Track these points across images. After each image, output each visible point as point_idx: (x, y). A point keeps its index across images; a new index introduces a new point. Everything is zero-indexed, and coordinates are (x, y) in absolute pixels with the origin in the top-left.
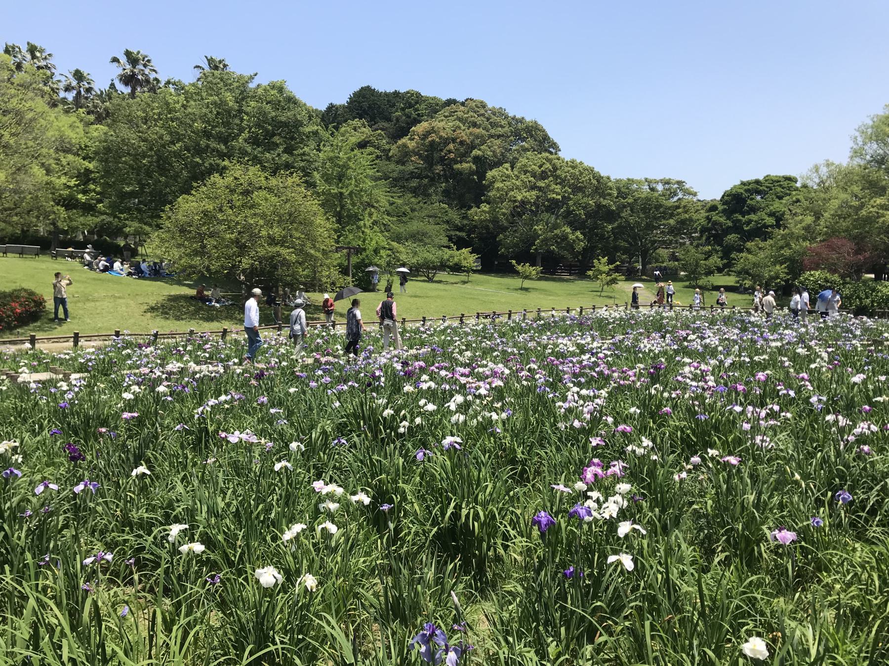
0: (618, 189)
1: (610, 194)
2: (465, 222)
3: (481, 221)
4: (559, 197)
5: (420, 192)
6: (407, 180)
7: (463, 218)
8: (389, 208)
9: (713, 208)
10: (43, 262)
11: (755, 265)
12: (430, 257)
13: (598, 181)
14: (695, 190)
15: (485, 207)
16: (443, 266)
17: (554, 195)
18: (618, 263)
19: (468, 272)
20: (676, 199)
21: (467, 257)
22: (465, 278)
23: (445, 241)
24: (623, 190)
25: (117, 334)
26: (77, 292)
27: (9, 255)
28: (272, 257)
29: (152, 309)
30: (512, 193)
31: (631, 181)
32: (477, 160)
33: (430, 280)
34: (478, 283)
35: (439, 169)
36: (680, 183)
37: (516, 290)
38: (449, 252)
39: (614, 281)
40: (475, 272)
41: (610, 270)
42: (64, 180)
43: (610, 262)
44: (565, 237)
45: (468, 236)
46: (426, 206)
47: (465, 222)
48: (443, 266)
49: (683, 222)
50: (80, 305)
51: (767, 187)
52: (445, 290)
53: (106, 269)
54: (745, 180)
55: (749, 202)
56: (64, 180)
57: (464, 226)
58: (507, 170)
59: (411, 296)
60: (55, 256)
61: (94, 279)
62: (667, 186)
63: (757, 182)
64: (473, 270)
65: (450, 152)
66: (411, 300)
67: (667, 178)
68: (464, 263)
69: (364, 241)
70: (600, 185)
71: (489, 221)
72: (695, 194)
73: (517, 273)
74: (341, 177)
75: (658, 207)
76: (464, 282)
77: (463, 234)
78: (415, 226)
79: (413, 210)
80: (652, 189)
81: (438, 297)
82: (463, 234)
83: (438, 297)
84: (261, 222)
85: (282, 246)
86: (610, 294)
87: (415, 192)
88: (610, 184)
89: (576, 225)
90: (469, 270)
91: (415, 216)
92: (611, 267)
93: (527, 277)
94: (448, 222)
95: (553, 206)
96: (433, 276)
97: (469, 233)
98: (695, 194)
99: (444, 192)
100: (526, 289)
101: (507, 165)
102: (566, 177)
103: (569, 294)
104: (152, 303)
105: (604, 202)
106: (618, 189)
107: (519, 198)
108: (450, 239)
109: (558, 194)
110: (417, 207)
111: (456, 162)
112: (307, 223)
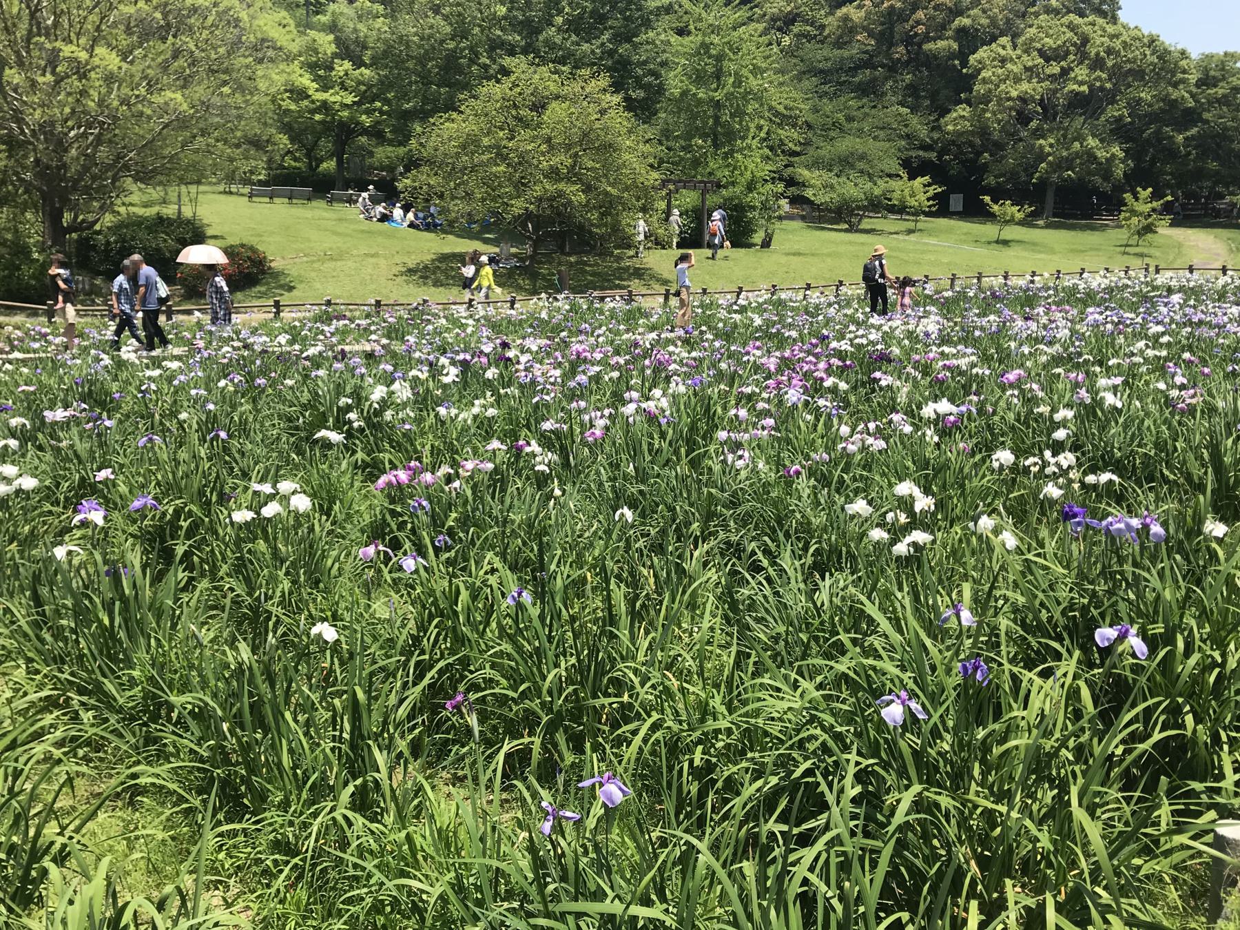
0: (1206, 71)
1: (1183, 81)
2: (936, 135)
3: (960, 134)
4: (1085, 88)
5: (867, 90)
7: (933, 129)
8: (811, 118)
15: (963, 110)
16: (878, 206)
17: (1075, 87)
18: (1169, 198)
19: (916, 214)
21: (919, 191)
22: (911, 225)
23: (893, 165)
25: (329, 303)
27: (276, 200)
28: (552, 199)
29: (411, 271)
32: (962, 33)
33: (852, 229)
35: (900, 51)
39: (1149, 229)
41: (1154, 210)
43: (1155, 196)
44: (1090, 156)
45: (939, 157)
47: (936, 135)
52: (850, 243)
53: (384, 218)
57: (936, 142)
58: (1004, 47)
60: (330, 202)
65: (918, 23)
66: (784, 259)
70: (1166, 65)
71: (972, 133)
74: (718, 75)
76: (910, 232)
77: (933, 155)
78: (845, 145)
79: (850, 119)
81: (829, 255)
83: (829, 255)
86: (1145, 251)
87: (864, 90)
88: (1184, 63)
90: (917, 213)
92: (1155, 204)
93: (1011, 221)
99: (908, 87)
100: (1006, 243)
101: (1004, 40)
103: (1072, 251)
105: (1175, 94)
107: (1014, 94)
108: (906, 164)
109: (1081, 83)
110: (858, 114)
111: (927, 38)
112: (608, 148)
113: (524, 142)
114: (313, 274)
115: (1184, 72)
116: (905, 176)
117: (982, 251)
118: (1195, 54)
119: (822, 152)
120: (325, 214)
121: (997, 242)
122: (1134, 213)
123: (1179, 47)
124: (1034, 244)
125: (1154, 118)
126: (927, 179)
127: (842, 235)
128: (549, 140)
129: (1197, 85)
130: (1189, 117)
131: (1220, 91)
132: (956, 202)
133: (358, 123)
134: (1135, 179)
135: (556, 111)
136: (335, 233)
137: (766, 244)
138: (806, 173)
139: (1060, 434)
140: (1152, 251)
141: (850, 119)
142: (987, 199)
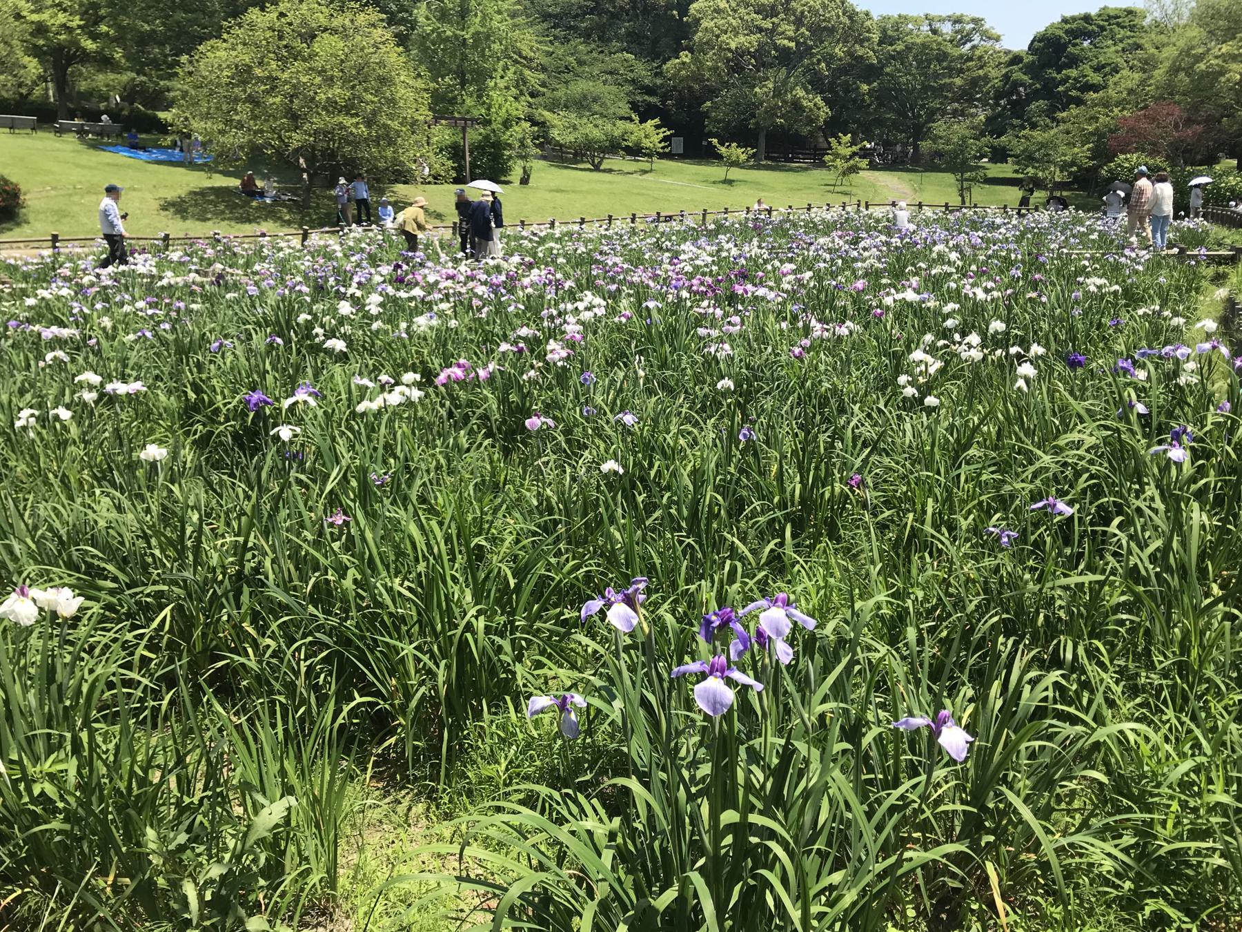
0: (884, 31)
1: (868, 39)
2: (659, 81)
4: (792, 44)
6: (577, 16)
7: (656, 75)
9: (1016, 59)
10: (41, 139)
11: (1043, 145)
12: (597, 134)
13: (850, 18)
14: (996, 31)
15: (685, 57)
16: (614, 147)
19: (650, 155)
20: (968, 46)
21: (650, 133)
22: (646, 166)
23: (625, 109)
24: (890, 33)
26: (80, 182)
30: (724, 37)
31: (904, 19)
33: (597, 168)
34: (663, 173)
36: (976, 21)
37: (714, 183)
38: (629, 126)
39: (854, 169)
40: (662, 156)
42: (62, 18)
46: (601, 56)
48: (614, 147)
49: (974, 82)
50: (76, 199)
51: (1099, 26)
54: (1068, 15)
55: (1070, 49)
56: (62, 18)
59: (551, 191)
61: (108, 164)
62: (958, 26)
63: (1087, 18)
64: (658, 153)
66: (549, 196)
67: (958, 14)
68: (646, 143)
69: (488, 109)
72: (997, 39)
73: (720, 157)
75: (942, 57)
76: (645, 172)
77: (653, 100)
78: (580, 87)
79: (581, 63)
80: (935, 32)
81: (588, 192)
82: (653, 100)
83: (588, 192)
84: (318, 80)
85: (347, 114)
87: (587, 35)
88: (868, 23)
89: (816, 83)
91: (583, 72)
92: (855, 148)
93: (736, 164)
94: (633, 81)
95: (786, 58)
96: (600, 163)
97: (664, 98)
98: (997, 39)
99: (629, 34)
100: (729, 182)
102: (802, 12)
103: (791, 189)
104: (171, 195)
105: (860, 51)
106: (884, 31)
107: (733, 46)
108: (634, 106)
113: (295, 73)
114: (75, 208)
115: (869, 31)
116: (637, 119)
117: (714, 189)
118: (875, 15)
119: (558, 94)
120: (58, 145)
121: (562, 191)
122: (837, 155)
123: (864, 9)
124: (758, 183)
125: (843, 70)
126: (657, 121)
127: (588, 173)
128: (322, 72)
129: (880, 44)
130: (870, 72)
131: (900, 47)
132: (678, 144)
133: (79, 48)
134: (834, 127)
135: (326, 46)
136: (77, 166)
137: (525, 181)
138: (546, 114)
139: (950, 323)
140: (854, 190)
141: (581, 63)
142: (715, 141)
